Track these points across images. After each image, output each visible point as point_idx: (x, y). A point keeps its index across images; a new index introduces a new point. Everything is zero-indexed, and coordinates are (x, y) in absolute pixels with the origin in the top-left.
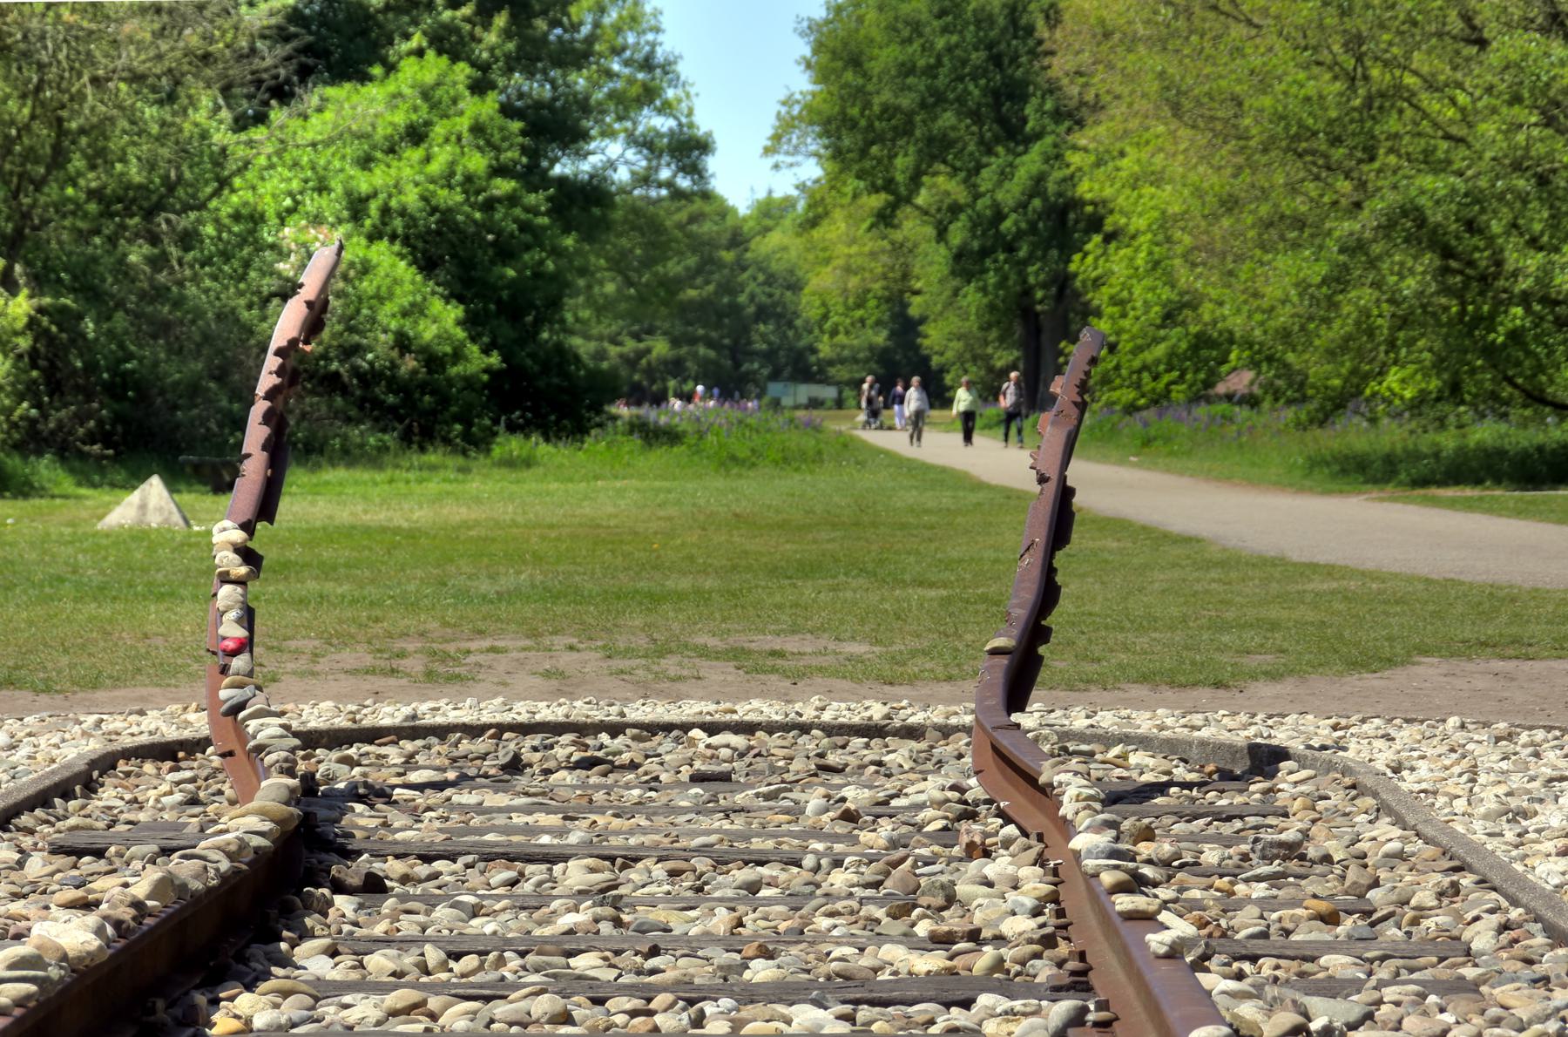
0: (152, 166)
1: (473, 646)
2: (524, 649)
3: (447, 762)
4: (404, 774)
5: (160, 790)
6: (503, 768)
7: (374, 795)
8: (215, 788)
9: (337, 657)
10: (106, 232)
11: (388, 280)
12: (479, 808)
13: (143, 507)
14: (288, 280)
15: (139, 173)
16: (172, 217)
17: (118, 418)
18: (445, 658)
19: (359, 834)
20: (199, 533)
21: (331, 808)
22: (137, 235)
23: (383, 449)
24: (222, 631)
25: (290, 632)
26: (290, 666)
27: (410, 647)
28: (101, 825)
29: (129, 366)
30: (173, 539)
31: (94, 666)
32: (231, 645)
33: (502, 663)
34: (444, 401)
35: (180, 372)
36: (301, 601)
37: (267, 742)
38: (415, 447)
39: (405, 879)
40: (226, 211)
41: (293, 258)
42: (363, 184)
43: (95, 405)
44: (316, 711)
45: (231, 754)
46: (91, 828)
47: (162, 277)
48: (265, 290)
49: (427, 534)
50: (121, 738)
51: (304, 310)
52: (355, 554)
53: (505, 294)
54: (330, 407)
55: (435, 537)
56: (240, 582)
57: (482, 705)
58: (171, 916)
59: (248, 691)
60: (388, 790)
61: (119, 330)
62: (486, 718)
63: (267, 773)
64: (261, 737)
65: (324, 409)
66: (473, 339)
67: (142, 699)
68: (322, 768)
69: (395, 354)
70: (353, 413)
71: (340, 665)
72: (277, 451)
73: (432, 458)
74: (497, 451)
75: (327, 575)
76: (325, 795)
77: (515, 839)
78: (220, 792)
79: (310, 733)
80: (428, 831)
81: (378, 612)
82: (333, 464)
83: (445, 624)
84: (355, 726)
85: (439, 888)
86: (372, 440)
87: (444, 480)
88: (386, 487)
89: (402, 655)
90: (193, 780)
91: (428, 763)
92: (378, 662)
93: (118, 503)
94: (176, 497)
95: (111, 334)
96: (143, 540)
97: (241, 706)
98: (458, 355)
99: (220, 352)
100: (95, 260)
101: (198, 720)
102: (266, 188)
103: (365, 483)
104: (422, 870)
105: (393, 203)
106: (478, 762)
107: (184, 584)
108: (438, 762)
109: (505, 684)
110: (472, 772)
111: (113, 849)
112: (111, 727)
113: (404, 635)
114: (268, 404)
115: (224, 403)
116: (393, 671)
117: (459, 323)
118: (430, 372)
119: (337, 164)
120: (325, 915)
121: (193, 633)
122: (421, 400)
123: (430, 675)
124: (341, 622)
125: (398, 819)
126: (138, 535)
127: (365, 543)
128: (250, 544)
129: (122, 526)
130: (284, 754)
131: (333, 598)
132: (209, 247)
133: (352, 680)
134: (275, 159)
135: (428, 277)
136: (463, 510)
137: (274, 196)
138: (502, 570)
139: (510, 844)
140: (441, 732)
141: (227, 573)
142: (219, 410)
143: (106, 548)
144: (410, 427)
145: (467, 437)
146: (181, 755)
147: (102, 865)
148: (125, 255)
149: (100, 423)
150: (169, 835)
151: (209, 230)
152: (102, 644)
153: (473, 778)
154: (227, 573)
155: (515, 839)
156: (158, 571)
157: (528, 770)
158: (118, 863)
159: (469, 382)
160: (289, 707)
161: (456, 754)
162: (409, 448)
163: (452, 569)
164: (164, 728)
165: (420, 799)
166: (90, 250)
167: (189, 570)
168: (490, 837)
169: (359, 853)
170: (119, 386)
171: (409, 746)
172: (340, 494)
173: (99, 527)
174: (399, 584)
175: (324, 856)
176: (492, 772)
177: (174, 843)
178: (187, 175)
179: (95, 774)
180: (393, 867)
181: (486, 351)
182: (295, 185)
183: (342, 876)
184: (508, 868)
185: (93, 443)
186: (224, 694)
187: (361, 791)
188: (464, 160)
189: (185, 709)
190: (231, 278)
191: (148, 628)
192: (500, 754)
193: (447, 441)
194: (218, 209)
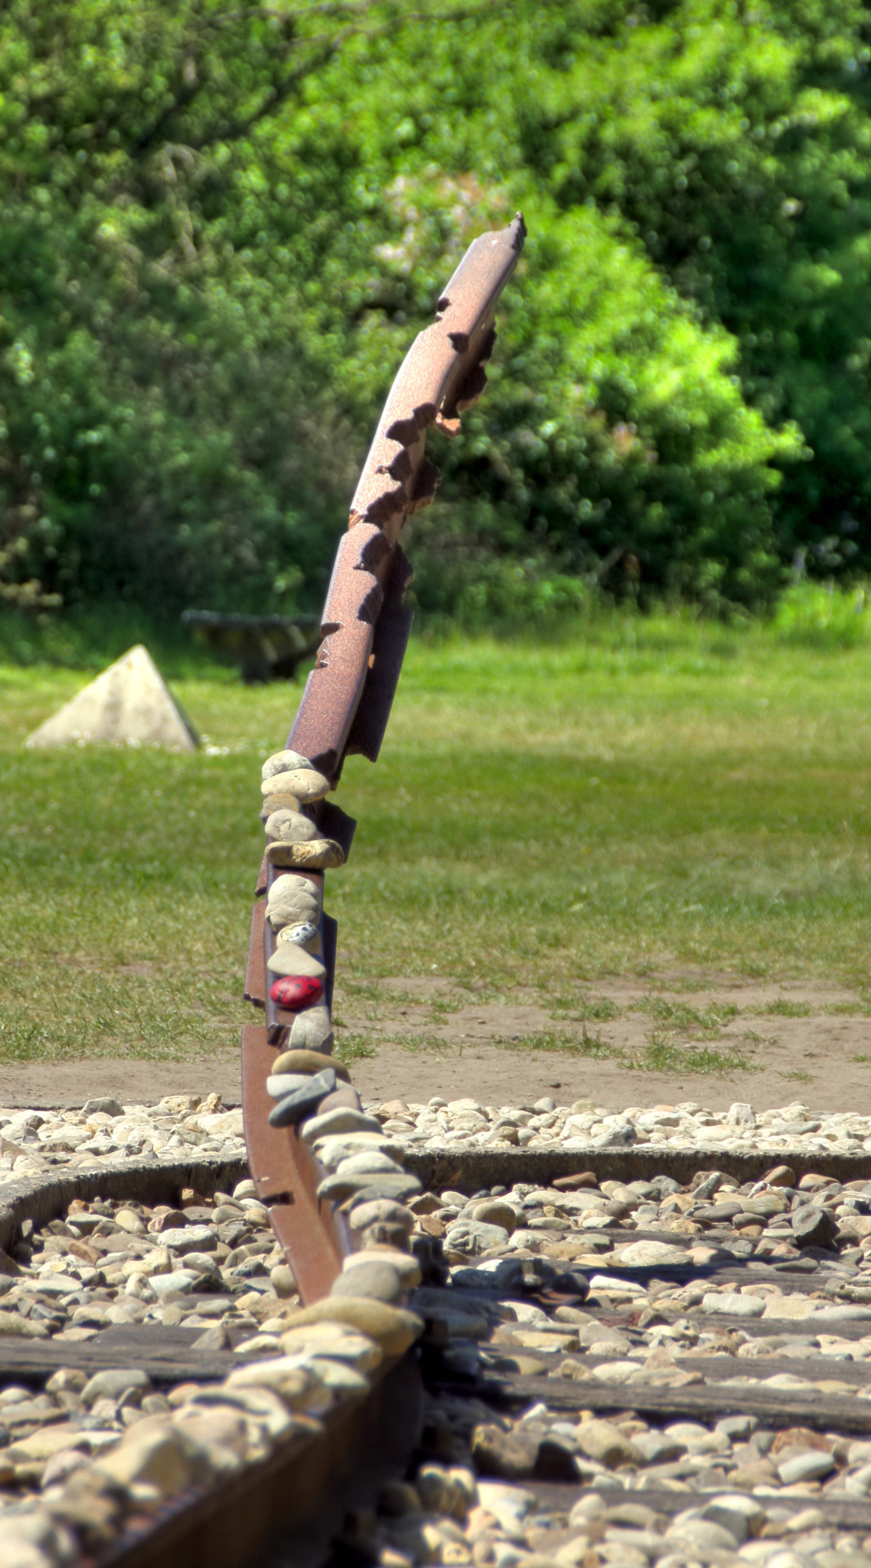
0: (148, 51)
1: (742, 999)
2: (840, 1010)
3: (692, 1227)
4: (608, 1248)
5: (145, 1264)
6: (801, 1243)
7: (552, 1287)
8: (251, 1261)
9: (481, 1012)
10: (60, 177)
11: (591, 285)
12: (755, 1323)
13: (114, 707)
14: (399, 278)
15: (126, 68)
16: (185, 152)
17: (71, 535)
18: (689, 1022)
19: (526, 1365)
20: (216, 760)
21: (472, 1309)
22: (119, 188)
23: (567, 606)
24: (275, 963)
25: (391, 961)
26: (392, 1028)
27: (621, 997)
28: (36, 1326)
29: (94, 436)
30: (168, 770)
31: (24, 1015)
32: (291, 990)
33: (799, 1036)
34: (689, 516)
35: (188, 448)
36: (412, 900)
37: (355, 1179)
38: (630, 603)
39: (614, 1458)
40: (287, 143)
41: (410, 236)
42: (553, 96)
43: (28, 510)
44: (441, 1116)
45: (285, 1199)
46: (17, 1333)
47: (161, 268)
48: (355, 297)
49: (650, 775)
50: (74, 1158)
51: (447, 353)
52: (512, 809)
53: (818, 319)
54: (469, 523)
55: (665, 781)
56: (310, 869)
57: (761, 1118)
58: (177, 1520)
59: (322, 1080)
60: (579, 1278)
61: (78, 369)
62: (768, 1145)
63: (355, 1241)
64: (345, 1172)
65: (457, 528)
66: (749, 399)
67: (113, 1082)
68: (453, 1230)
69: (597, 423)
70: (513, 533)
71: (488, 1029)
72: (387, 622)
73: (661, 624)
74: (788, 616)
75: (459, 849)
76: (459, 1283)
77: (828, 1387)
78: (260, 1271)
79: (430, 1159)
80: (655, 1364)
81: (557, 927)
82: (470, 630)
83: (689, 955)
84: (516, 1151)
85: (681, 1477)
86: (547, 589)
87: (685, 670)
88: (572, 681)
89: (604, 1013)
90: (208, 1244)
91: (654, 1227)
92: (559, 1026)
93: (67, 698)
94: (176, 688)
95: (62, 376)
96: (112, 770)
97: (309, 1108)
98: (719, 428)
99: (265, 414)
100: (36, 232)
101: (220, 1128)
102: (364, 100)
103: (532, 672)
104: (648, 1441)
105: (609, 134)
106: (752, 1230)
107: (188, 858)
108: (673, 1227)
109: (804, 1078)
110: (740, 1249)
111: (60, 1376)
112: (57, 1135)
113: (608, 973)
114: (372, 530)
115: (269, 510)
116: (588, 1043)
117: (726, 370)
118: (663, 458)
119: (503, 57)
120: (462, 1521)
121: (209, 956)
122: (643, 514)
123: (659, 1054)
124: (486, 944)
125: (601, 1339)
126: (103, 761)
127: (530, 787)
128: (333, 798)
129: (73, 742)
130: (388, 1205)
131: (471, 896)
132: (252, 212)
133: (510, 1059)
134: (383, 44)
135: (672, 280)
136: (721, 730)
137: (380, 116)
138: (795, 849)
139: (818, 1398)
140: (682, 1168)
141: (288, 851)
142: (259, 525)
143: (44, 783)
144: (620, 565)
145: (731, 589)
146: (187, 1194)
147: (39, 1407)
148: (94, 224)
149: (37, 542)
150: (167, 1351)
151: (253, 178)
152: (39, 973)
153: (742, 1262)
154: (288, 851)
155: (828, 1387)
156: (141, 830)
157: (849, 1251)
158: (70, 1402)
159: (739, 480)
160: (391, 1107)
161: (708, 1211)
162: (619, 602)
163: (696, 844)
164: (156, 1141)
165: (642, 1299)
166: (27, 213)
167: (197, 832)
168: (779, 1382)
169: (526, 1402)
170: (73, 476)
171: (618, 1192)
172: (483, 692)
173: (32, 741)
174: (596, 871)
175: (459, 1405)
176: (780, 1250)
177: (177, 1369)
178: (218, 71)
179: (27, 1226)
180: (591, 1434)
181: (774, 422)
182: (421, 96)
183: (495, 1447)
184: (815, 1446)
185: (23, 580)
186: (276, 1084)
187: (529, 1278)
188: (749, 53)
189: (195, 1104)
190: (292, 271)
191: (126, 944)
192: (797, 1215)
193: (691, 594)
194: (271, 139)
